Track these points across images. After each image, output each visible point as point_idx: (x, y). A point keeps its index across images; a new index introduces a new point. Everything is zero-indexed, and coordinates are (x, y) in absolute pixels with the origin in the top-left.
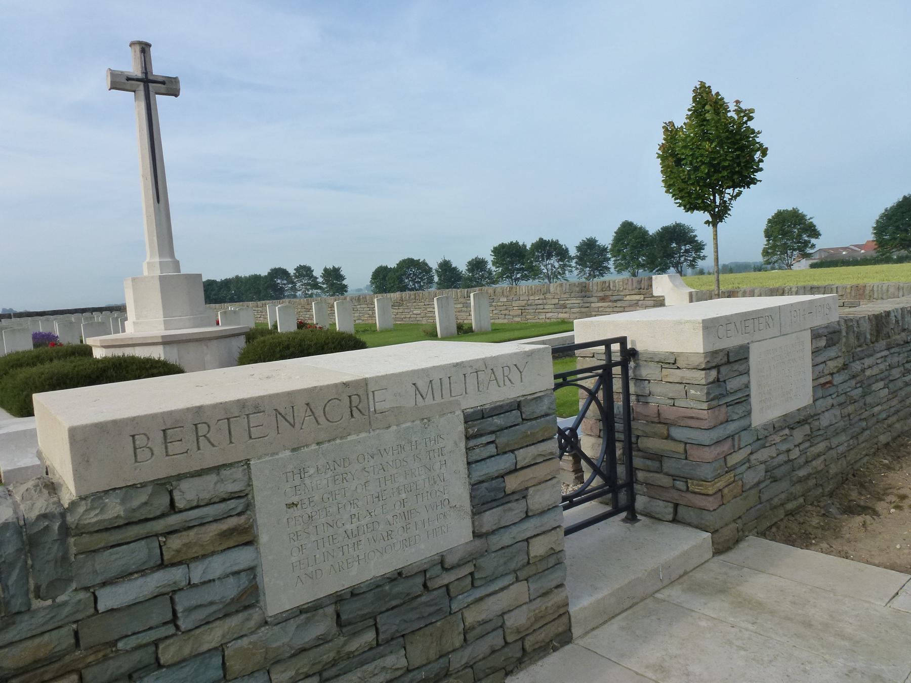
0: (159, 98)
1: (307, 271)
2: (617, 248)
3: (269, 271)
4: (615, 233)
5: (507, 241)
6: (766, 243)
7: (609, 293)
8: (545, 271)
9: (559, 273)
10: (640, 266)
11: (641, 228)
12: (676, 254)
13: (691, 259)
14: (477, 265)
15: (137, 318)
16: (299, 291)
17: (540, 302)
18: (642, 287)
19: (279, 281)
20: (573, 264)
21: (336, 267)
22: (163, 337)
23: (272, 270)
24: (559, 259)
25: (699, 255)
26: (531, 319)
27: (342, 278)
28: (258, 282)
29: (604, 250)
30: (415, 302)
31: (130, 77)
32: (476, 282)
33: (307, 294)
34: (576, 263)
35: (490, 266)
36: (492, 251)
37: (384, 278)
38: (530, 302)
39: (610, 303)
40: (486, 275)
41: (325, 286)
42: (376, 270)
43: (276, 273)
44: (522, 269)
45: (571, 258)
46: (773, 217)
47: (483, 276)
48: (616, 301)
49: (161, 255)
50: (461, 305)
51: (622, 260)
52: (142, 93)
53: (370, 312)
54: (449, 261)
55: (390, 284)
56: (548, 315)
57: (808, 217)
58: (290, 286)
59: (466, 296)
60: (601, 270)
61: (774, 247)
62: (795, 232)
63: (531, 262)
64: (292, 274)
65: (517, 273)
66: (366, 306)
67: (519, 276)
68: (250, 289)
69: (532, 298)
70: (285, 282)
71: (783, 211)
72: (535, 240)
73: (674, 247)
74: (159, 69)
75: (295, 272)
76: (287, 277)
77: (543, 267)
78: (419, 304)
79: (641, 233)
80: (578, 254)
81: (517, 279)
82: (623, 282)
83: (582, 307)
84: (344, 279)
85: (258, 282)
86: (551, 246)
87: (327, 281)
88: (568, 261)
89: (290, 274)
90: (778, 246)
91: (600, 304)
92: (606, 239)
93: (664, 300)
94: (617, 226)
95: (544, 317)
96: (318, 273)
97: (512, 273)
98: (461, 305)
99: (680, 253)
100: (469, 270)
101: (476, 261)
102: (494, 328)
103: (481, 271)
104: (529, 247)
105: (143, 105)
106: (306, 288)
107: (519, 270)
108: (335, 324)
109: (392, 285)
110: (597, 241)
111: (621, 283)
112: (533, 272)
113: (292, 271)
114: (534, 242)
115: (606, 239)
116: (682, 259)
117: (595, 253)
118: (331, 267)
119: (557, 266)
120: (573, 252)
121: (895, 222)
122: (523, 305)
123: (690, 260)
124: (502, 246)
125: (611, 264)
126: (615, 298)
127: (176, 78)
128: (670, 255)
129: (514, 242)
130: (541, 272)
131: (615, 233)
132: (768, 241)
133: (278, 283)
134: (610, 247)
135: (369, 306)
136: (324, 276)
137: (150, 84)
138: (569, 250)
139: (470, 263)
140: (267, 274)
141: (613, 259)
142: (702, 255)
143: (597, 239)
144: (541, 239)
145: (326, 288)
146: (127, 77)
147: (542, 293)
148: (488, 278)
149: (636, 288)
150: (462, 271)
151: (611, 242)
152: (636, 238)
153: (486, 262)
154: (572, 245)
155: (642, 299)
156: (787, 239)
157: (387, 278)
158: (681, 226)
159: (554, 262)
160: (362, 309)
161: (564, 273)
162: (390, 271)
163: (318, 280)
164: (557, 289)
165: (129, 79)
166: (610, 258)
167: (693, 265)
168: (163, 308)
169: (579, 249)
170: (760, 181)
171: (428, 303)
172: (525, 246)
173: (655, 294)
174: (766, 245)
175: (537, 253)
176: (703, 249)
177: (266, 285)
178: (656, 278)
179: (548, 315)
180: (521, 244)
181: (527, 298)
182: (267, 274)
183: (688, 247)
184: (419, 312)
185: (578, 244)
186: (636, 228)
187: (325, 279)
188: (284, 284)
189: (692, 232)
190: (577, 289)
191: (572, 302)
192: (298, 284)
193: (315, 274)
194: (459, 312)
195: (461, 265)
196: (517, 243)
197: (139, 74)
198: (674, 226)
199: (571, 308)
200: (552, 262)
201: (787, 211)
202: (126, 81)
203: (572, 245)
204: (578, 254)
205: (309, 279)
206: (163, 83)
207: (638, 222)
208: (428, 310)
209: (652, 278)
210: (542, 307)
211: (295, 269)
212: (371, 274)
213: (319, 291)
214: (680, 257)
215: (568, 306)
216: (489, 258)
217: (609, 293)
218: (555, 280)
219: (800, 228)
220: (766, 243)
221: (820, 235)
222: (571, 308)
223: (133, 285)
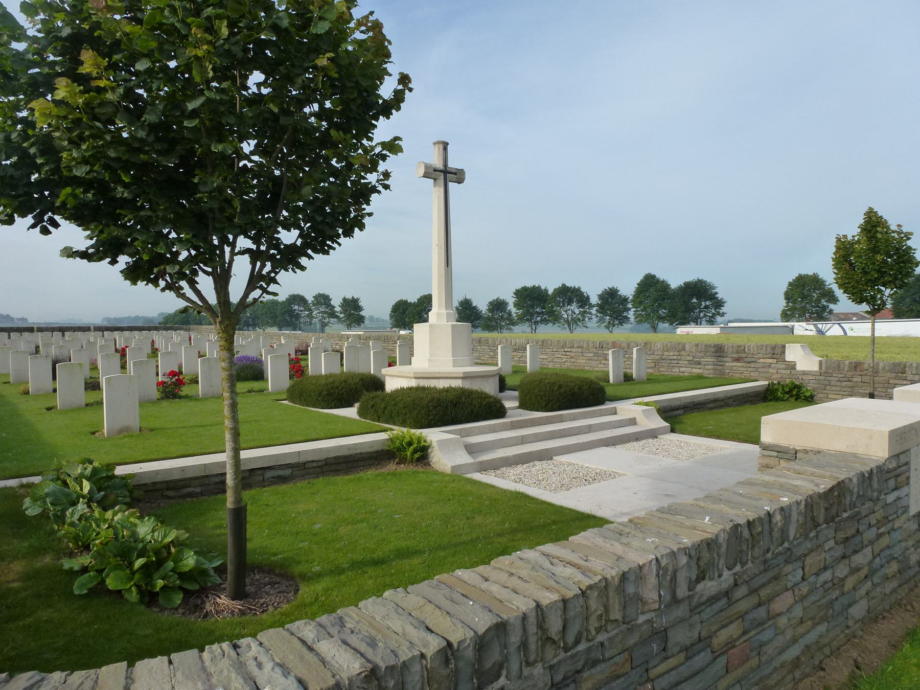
1: (326, 299)
2: (638, 300)
4: (638, 284)
5: (529, 284)
6: (785, 305)
7: (744, 355)
8: (565, 316)
9: (579, 319)
10: (662, 319)
11: (663, 281)
12: (696, 309)
13: (711, 315)
14: (498, 306)
15: (431, 356)
17: (675, 357)
18: (776, 353)
19: (296, 307)
20: (594, 311)
24: (579, 306)
25: (719, 312)
26: (664, 370)
27: (360, 309)
28: (275, 307)
29: (625, 300)
33: (323, 322)
34: (597, 310)
35: (511, 308)
36: (514, 294)
37: (404, 312)
38: (664, 357)
39: (744, 364)
40: (506, 316)
41: (342, 316)
42: (396, 304)
43: (294, 299)
45: (591, 306)
46: (793, 280)
47: (502, 316)
48: (749, 362)
50: (592, 355)
51: (642, 310)
52: (442, 181)
53: (492, 354)
56: (682, 369)
57: (827, 283)
58: (307, 313)
59: (598, 347)
60: (621, 319)
61: (793, 309)
62: (814, 296)
63: (552, 307)
65: (537, 317)
66: (488, 348)
67: (539, 319)
68: (267, 314)
69: (666, 353)
70: (302, 309)
71: (804, 275)
72: (558, 285)
73: (695, 303)
74: (453, 164)
75: (313, 299)
77: (563, 313)
79: (664, 286)
80: (599, 303)
81: (536, 323)
82: (758, 348)
83: (716, 365)
84: (362, 310)
85: (275, 307)
86: (573, 292)
87: (344, 311)
88: (589, 308)
90: (797, 308)
91: (735, 364)
92: (628, 289)
93: (795, 365)
94: (639, 278)
95: (677, 370)
96: (336, 302)
97: (532, 315)
99: (700, 308)
100: (489, 310)
101: (497, 302)
104: (550, 292)
105: (442, 190)
107: (538, 313)
109: (412, 319)
110: (618, 291)
111: (756, 348)
112: (553, 317)
113: (310, 299)
115: (628, 289)
116: (702, 315)
117: (617, 303)
118: (350, 298)
119: (577, 313)
120: (594, 300)
121: (914, 295)
122: (658, 358)
123: (710, 317)
124: (525, 289)
125: (631, 314)
126: (749, 360)
127: (462, 170)
128: (689, 309)
129: (537, 286)
130: (561, 317)
131: (638, 284)
132: (788, 303)
134: (631, 297)
136: (342, 306)
138: (590, 297)
139: (491, 303)
140: (284, 300)
141: (633, 310)
142: (721, 311)
143: (618, 289)
144: (564, 285)
145: (343, 317)
147: (677, 350)
148: (507, 319)
149: (770, 353)
150: (482, 311)
151: (633, 293)
152: (657, 291)
153: (507, 304)
154: (594, 295)
155: (775, 362)
156: (807, 303)
158: (703, 283)
159: (574, 308)
163: (335, 309)
164: (692, 348)
165: (435, 170)
166: (630, 309)
167: (712, 321)
168: (453, 348)
169: (601, 297)
171: (556, 350)
172: (546, 291)
173: (787, 359)
174: (785, 307)
176: (723, 306)
177: (283, 310)
178: (789, 347)
179: (682, 369)
180: (543, 288)
181: (662, 354)
182: (284, 300)
183: (708, 303)
184: (545, 357)
185: (600, 293)
186: (658, 281)
188: (301, 311)
189: (714, 289)
190: (713, 350)
191: (707, 360)
192: (315, 312)
194: (589, 360)
195: (482, 305)
196: (539, 287)
197: (440, 166)
198: (696, 282)
199: (705, 365)
201: (807, 275)
203: (594, 295)
204: (599, 303)
205: (327, 308)
206: (455, 174)
207: (661, 275)
208: (556, 356)
209: (785, 346)
210: (676, 362)
211: (314, 297)
213: (335, 320)
214: (700, 312)
215: (702, 363)
216: (511, 300)
217: (744, 355)
218: (574, 326)
219: (819, 293)
220: (785, 305)
221: (838, 301)
222: (705, 365)
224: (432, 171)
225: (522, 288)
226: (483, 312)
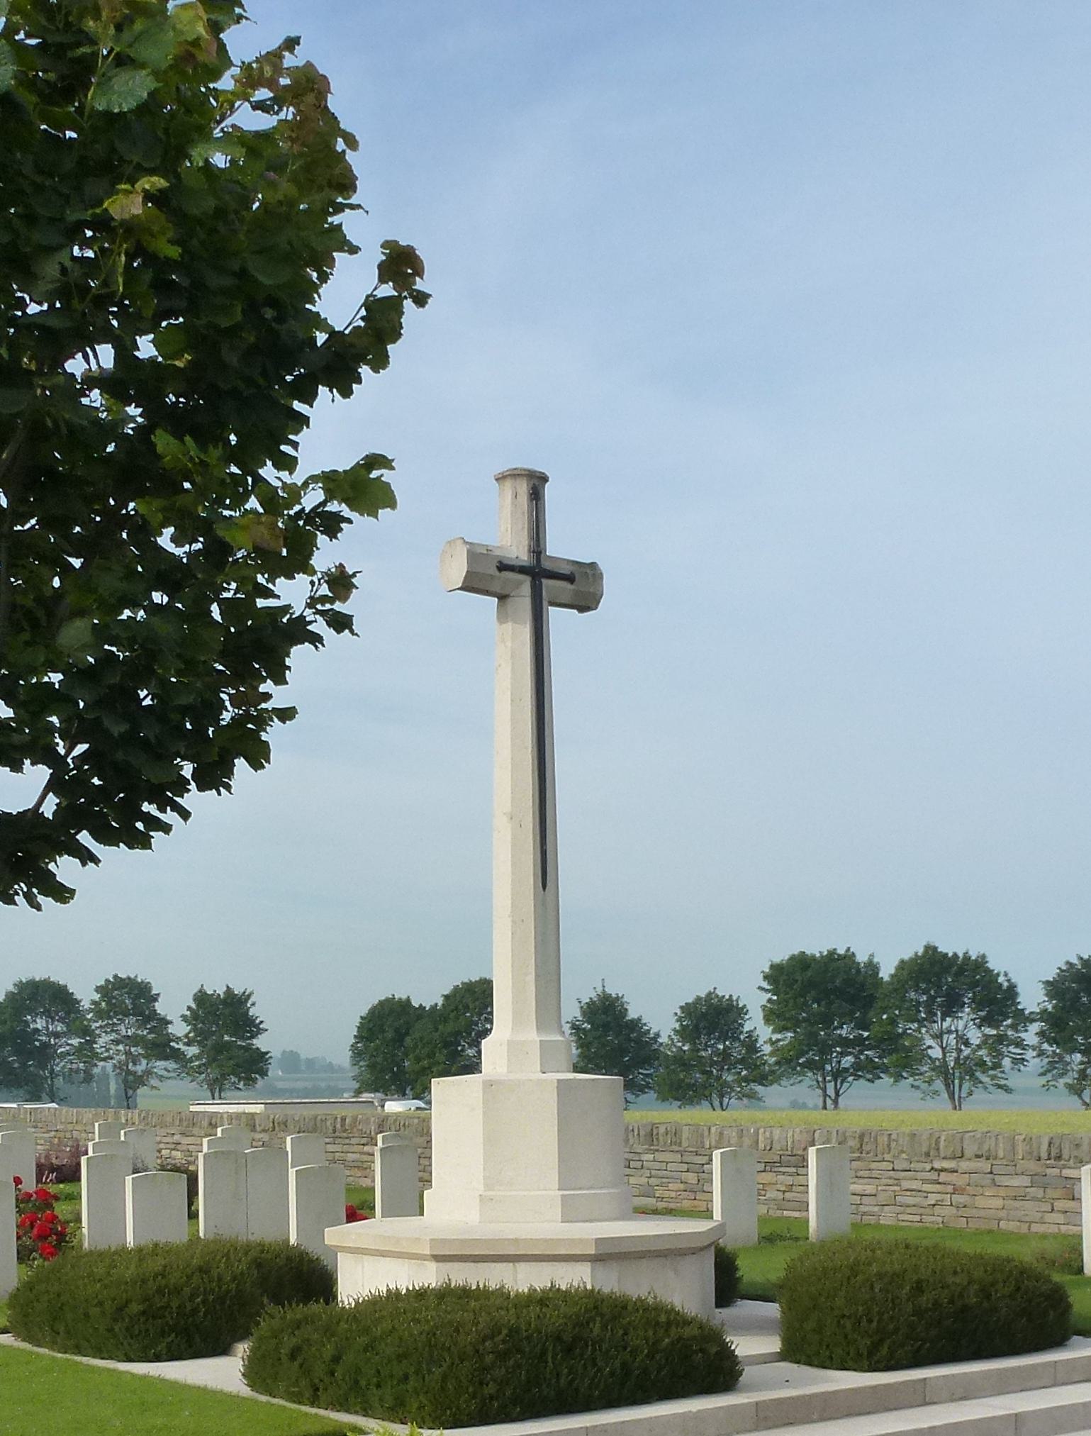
0: (553, 611)
1: (138, 997)
3: (11, 988)
5: (816, 947)
8: (936, 1053)
9: (981, 1064)
16: (104, 1059)
19: (40, 1024)
21: (237, 991)
22: (599, 1241)
23: (21, 986)
27: (250, 1027)
30: (858, 1159)
31: (505, 562)
32: (704, 1072)
33: (129, 1072)
34: (1041, 1034)
35: (756, 1024)
36: (766, 977)
40: (738, 1052)
41: (192, 1051)
43: (33, 997)
44: (859, 1041)
45: (1022, 1019)
47: (726, 1054)
49: (540, 1027)
50: (1025, 1181)
53: (691, 1178)
54: (618, 998)
55: (418, 1059)
59: (1044, 1155)
63: (893, 1022)
64: (86, 1004)
65: (842, 1054)
67: (848, 1061)
70: (60, 1027)
72: (911, 948)
74: (559, 547)
75: (97, 997)
76: (68, 1013)
78: (874, 1165)
80: (1050, 1008)
84: (260, 1031)
87: (200, 1035)
88: (1014, 1027)
89: (78, 1002)
97: (825, 1049)
98: (1025, 1181)
100: (683, 1033)
102: (766, 1232)
103: (723, 1038)
104: (886, 973)
106: (128, 1053)
108: (373, 1189)
113: (86, 995)
114: (907, 956)
120: (1032, 998)
124: (802, 962)
127: (593, 565)
129: (841, 951)
130: (923, 1056)
133: (37, 1030)
135: (686, 1159)
136: (193, 1018)
137: (544, 581)
138: (1019, 990)
139: (688, 1010)
144: (931, 950)
145: (197, 1057)
146: (500, 562)
148: (742, 1061)
150: (658, 1035)
157: (408, 1040)
160: (657, 1165)
161: (997, 1066)
162: (419, 1017)
163: (171, 1029)
165: (503, 567)
168: (561, 1160)
169: (1054, 988)
170: (715, 988)
171: (905, 1165)
172: (873, 967)
175: (912, 995)
180: (862, 958)
184: (870, 1189)
185: (1051, 975)
187: (195, 1029)
188: (57, 1035)
192: (103, 1040)
193: (160, 1007)
194: (1015, 1198)
196: (849, 957)
197: (518, 551)
200: (961, 1024)
202: (497, 573)
204: (1050, 1008)
206: (570, 578)
208: (906, 1185)
211: (98, 989)
212: (357, 1021)
213: (171, 1065)
223: (485, 1102)
224: (493, 571)
225: (793, 958)
226: (663, 1039)
